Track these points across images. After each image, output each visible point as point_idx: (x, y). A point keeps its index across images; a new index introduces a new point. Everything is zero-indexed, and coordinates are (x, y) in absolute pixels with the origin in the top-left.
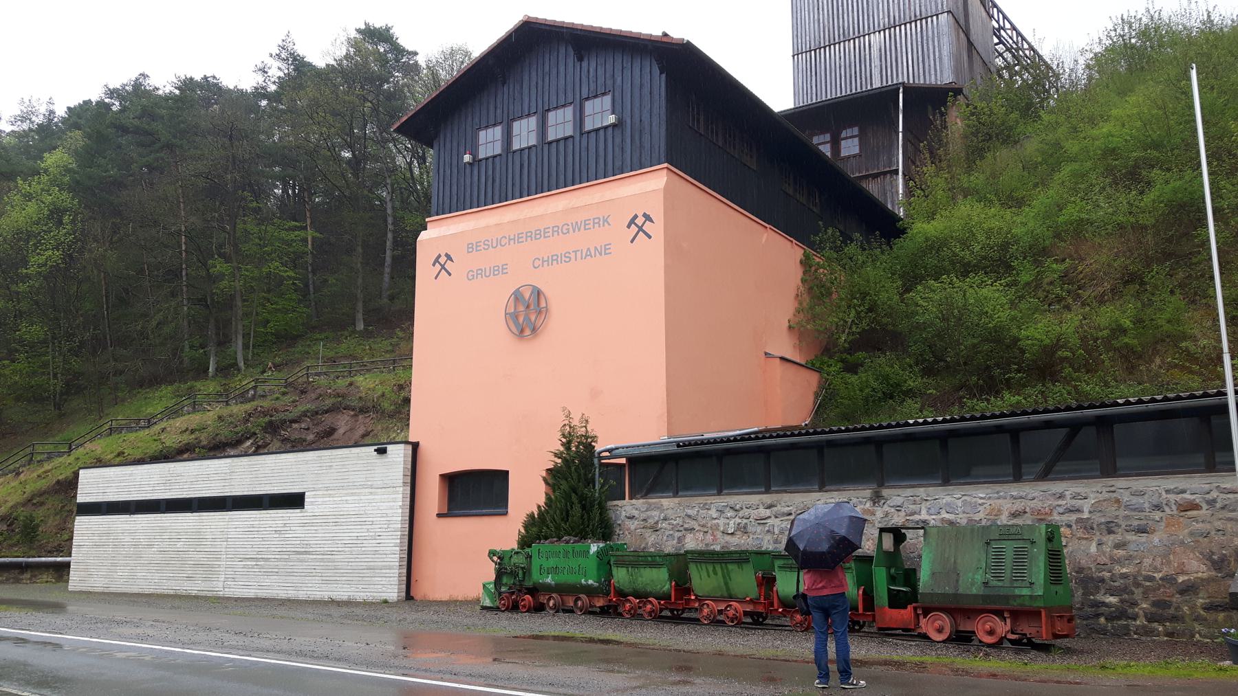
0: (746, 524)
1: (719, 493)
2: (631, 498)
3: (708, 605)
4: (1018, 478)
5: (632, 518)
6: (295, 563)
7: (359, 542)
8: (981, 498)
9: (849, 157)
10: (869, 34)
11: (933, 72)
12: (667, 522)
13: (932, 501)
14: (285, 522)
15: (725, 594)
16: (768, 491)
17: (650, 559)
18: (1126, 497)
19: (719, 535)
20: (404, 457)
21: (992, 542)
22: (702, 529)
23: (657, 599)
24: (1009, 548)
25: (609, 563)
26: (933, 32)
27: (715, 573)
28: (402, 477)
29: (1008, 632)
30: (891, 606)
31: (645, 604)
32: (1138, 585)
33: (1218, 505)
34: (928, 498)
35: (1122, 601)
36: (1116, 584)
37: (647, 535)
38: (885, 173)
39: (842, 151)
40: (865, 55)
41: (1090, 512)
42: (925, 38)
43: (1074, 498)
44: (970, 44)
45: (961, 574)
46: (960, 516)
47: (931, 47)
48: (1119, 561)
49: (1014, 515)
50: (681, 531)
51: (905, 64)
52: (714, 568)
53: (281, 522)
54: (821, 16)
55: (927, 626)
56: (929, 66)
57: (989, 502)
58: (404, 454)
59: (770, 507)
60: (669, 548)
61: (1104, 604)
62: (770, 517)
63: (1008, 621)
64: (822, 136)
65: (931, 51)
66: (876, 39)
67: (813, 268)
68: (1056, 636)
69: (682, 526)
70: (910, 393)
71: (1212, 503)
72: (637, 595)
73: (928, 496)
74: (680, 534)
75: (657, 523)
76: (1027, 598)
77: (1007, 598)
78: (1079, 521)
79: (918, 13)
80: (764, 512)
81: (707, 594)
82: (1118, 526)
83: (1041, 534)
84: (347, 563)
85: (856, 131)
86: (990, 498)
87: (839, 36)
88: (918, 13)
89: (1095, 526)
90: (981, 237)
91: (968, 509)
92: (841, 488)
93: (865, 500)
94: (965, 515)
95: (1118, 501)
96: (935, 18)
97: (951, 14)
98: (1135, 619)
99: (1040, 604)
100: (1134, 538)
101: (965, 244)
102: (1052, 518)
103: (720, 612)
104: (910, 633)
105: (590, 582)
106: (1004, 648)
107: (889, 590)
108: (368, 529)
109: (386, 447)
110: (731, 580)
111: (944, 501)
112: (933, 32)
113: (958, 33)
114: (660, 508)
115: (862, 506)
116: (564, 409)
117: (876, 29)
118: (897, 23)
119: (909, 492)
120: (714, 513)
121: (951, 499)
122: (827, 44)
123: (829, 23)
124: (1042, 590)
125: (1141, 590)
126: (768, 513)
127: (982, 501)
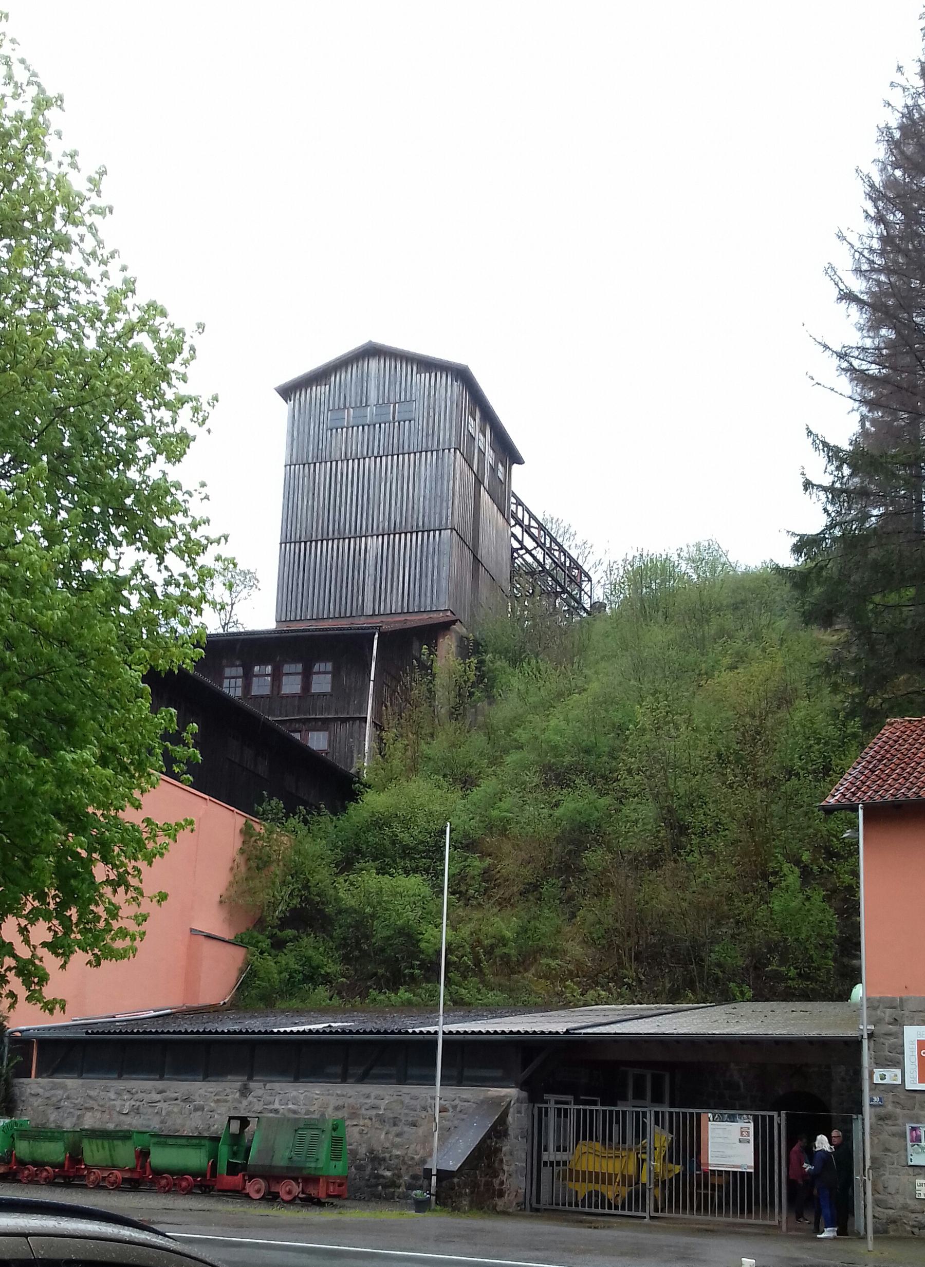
0: (139, 1106)
1: (120, 1077)
3: (94, 1173)
4: (344, 1081)
9: (319, 694)
10: (366, 537)
11: (429, 594)
15: (110, 1164)
16: (161, 1078)
17: (49, 1134)
18: (407, 1100)
19: (115, 1115)
22: (100, 1108)
23: (52, 1167)
24: (308, 1133)
25: (12, 1136)
26: (434, 549)
27: (103, 1148)
30: (228, 1174)
31: (41, 1172)
32: (404, 1163)
33: (458, 1109)
35: (394, 1175)
36: (392, 1162)
37: (50, 1111)
38: (354, 719)
39: (313, 686)
40: (360, 560)
41: (385, 1109)
42: (425, 554)
43: (375, 1098)
44: (476, 560)
47: (430, 565)
48: (394, 1146)
49: (337, 1108)
51: (401, 579)
52: (103, 1143)
54: (316, 503)
55: (250, 1188)
56: (426, 586)
57: (322, 1097)
60: (68, 1125)
61: (383, 1177)
62: (159, 1101)
63: (301, 1185)
64: (293, 666)
65: (430, 570)
66: (373, 544)
67: (253, 839)
68: (329, 1196)
70: (327, 980)
71: (455, 1107)
72: (35, 1163)
73: (281, 1090)
74: (79, 1112)
77: (301, 1169)
78: (378, 1115)
79: (421, 524)
81: (94, 1164)
82: (401, 1121)
85: (329, 666)
87: (334, 531)
88: (421, 524)
89: (386, 1120)
90: (421, 821)
92: (220, 1079)
95: (402, 1102)
96: (437, 532)
97: (454, 532)
98: (399, 1188)
100: (409, 1130)
101: (406, 824)
103: (104, 1178)
104: (239, 1194)
107: (229, 1162)
112: (434, 549)
113: (462, 551)
114: (64, 1087)
117: (375, 532)
118: (397, 531)
120: (112, 1095)
122: (320, 537)
123: (323, 513)
125: (406, 1167)
126: (158, 1097)
127: (318, 1097)
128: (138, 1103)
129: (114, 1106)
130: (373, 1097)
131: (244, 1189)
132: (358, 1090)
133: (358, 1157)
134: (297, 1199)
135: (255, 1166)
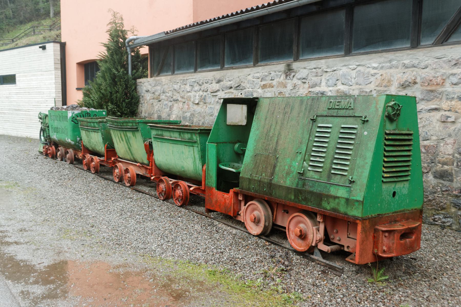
0: (205, 96)
1: (195, 71)
2: (151, 77)
4: (416, 45)
5: (147, 91)
6: (15, 116)
7: (38, 104)
8: (374, 68)
12: (164, 94)
13: (331, 73)
14: (10, 92)
16: (222, 68)
20: (54, 51)
21: (319, 119)
28: (53, 64)
29: (320, 241)
34: (328, 70)
45: (280, 160)
46: (353, 87)
49: (404, 86)
50: (172, 101)
53: (8, 92)
57: (381, 72)
58: (54, 49)
59: (219, 81)
62: (218, 90)
69: (172, 97)
73: (328, 67)
75: (159, 95)
76: (343, 202)
77: (320, 197)
80: (216, 86)
83: (377, 109)
84: (34, 117)
86: (382, 68)
91: (361, 80)
93: (280, 73)
94: (358, 87)
99: (356, 212)
102: (443, 89)
105: (69, 141)
106: (313, 260)
108: (42, 97)
109: (45, 46)
110: (131, 146)
111: (341, 72)
114: (160, 84)
115: (278, 80)
116: (109, 10)
119: (313, 64)
120: (188, 88)
121: (346, 70)
124: (363, 194)
127: (375, 71)
128: (205, 93)
129: (190, 97)
133: (439, 158)
135: (250, 180)
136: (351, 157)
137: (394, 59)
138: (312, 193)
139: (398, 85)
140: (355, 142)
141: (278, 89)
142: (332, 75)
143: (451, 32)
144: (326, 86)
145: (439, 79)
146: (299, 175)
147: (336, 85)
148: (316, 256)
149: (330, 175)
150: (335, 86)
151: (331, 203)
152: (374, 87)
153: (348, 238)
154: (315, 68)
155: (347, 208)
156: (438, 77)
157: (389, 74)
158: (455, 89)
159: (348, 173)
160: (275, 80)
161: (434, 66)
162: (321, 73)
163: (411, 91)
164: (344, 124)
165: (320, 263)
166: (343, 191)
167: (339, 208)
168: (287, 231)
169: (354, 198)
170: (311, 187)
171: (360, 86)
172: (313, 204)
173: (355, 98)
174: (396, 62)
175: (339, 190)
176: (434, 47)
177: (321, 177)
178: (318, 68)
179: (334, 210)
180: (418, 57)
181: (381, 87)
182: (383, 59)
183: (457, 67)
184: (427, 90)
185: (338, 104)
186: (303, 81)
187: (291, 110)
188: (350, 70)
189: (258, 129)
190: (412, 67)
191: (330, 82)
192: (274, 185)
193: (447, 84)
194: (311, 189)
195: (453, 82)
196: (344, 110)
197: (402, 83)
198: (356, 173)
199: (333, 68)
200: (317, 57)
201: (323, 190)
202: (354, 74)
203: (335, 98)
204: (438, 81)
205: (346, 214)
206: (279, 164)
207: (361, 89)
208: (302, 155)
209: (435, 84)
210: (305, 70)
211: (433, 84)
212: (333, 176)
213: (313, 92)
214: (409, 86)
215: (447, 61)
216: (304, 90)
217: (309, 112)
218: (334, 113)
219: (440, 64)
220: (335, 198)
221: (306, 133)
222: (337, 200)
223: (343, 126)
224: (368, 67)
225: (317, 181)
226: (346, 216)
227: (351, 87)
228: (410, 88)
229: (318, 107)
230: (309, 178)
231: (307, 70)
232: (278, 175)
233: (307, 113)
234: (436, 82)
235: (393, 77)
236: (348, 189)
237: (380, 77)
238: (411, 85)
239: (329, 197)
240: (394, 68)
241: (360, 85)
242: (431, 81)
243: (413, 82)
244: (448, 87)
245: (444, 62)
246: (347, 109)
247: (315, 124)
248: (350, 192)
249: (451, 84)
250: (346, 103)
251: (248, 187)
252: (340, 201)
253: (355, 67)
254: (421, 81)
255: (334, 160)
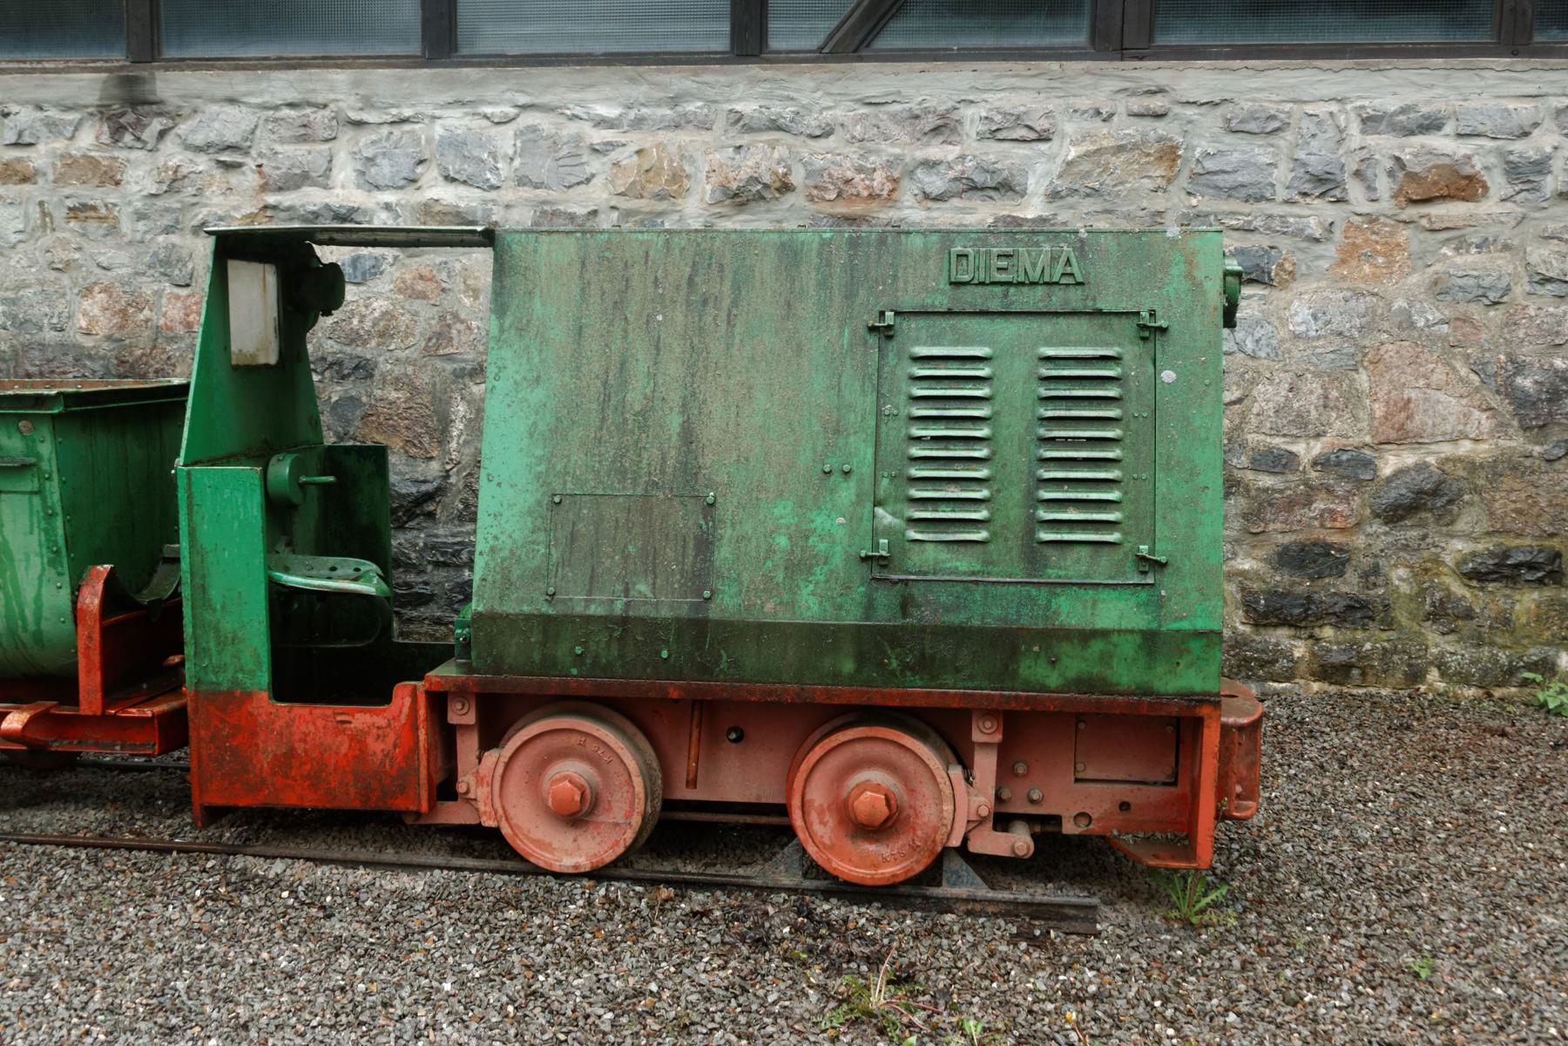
8: (602, 123)
13: (385, 130)
34: (365, 116)
43: (994, 135)
45: (726, 510)
46: (507, 195)
49: (739, 198)
57: (636, 139)
73: (368, 103)
76: (1128, 647)
86: (638, 123)
91: (542, 168)
94: (526, 193)
95: (1169, 154)
106: (945, 906)
107: (282, 601)
115: (60, 145)
119: (281, 85)
121: (466, 121)
130: (971, 129)
131: (446, 789)
132: (873, 90)
134: (956, 864)
136: (1121, 469)
137: (692, 95)
138: (960, 634)
139: (713, 192)
140: (1125, 412)
141: (67, 191)
142: (388, 139)
143: (886, 13)
144: (359, 186)
145: (879, 176)
146: (865, 567)
147: (414, 181)
148: (954, 885)
149: (1034, 553)
150: (411, 188)
151: (1066, 661)
152: (605, 196)
153: (1079, 785)
154: (291, 105)
155: (1149, 668)
156: (875, 170)
157: (673, 149)
158: (935, 214)
159: (1125, 534)
160: (41, 147)
161: (858, 131)
162: (331, 127)
163: (769, 216)
164: (1049, 344)
165: (978, 907)
166: (1121, 605)
167: (1108, 672)
168: (798, 821)
169: (1185, 625)
170: (947, 610)
171: (542, 193)
172: (971, 677)
173: (1081, 241)
174: (700, 104)
175: (1100, 606)
176: (825, 60)
177: (987, 563)
178: (310, 104)
179: (1085, 684)
180: (792, 94)
181: (642, 197)
182: (644, 88)
183: (941, 139)
184: (832, 216)
185: (1003, 263)
186: (225, 157)
187: (737, 289)
188: (485, 123)
189: (538, 380)
190: (770, 129)
191: (384, 170)
192: (722, 624)
193: (907, 197)
194: (955, 619)
195: (928, 190)
196: (1040, 290)
197: (734, 186)
198: (1162, 530)
199: (394, 111)
200: (272, 55)
201: (1020, 616)
202: (505, 140)
203: (979, 239)
204: (875, 183)
205: (1148, 692)
206: (727, 533)
207: (544, 202)
208: (860, 481)
209: (865, 193)
210: (231, 110)
211: (858, 195)
212: (1048, 551)
213: (289, 209)
214: (763, 198)
215: (906, 115)
216: (233, 200)
217: (850, 295)
218: (972, 298)
219: (881, 124)
220: (1086, 636)
221: (857, 385)
222: (1097, 646)
223: (1051, 352)
224: (576, 117)
225: (976, 582)
226: (1147, 699)
227: (493, 195)
228: (762, 206)
229: (895, 278)
230: (926, 573)
231: (244, 109)
232: (738, 580)
233: (837, 299)
234: (868, 187)
235: (692, 160)
236: (1143, 595)
237: (635, 158)
238: (767, 195)
239: (1052, 638)
240: (690, 126)
241: (537, 186)
242: (848, 182)
243: (778, 184)
244: (911, 207)
245: (893, 117)
246: (1057, 283)
247: (892, 346)
248: (1159, 604)
249: (920, 197)
250: (1043, 260)
251: (537, 657)
252: (1115, 646)
253: (512, 111)
254: (811, 182)
255: (1038, 488)
